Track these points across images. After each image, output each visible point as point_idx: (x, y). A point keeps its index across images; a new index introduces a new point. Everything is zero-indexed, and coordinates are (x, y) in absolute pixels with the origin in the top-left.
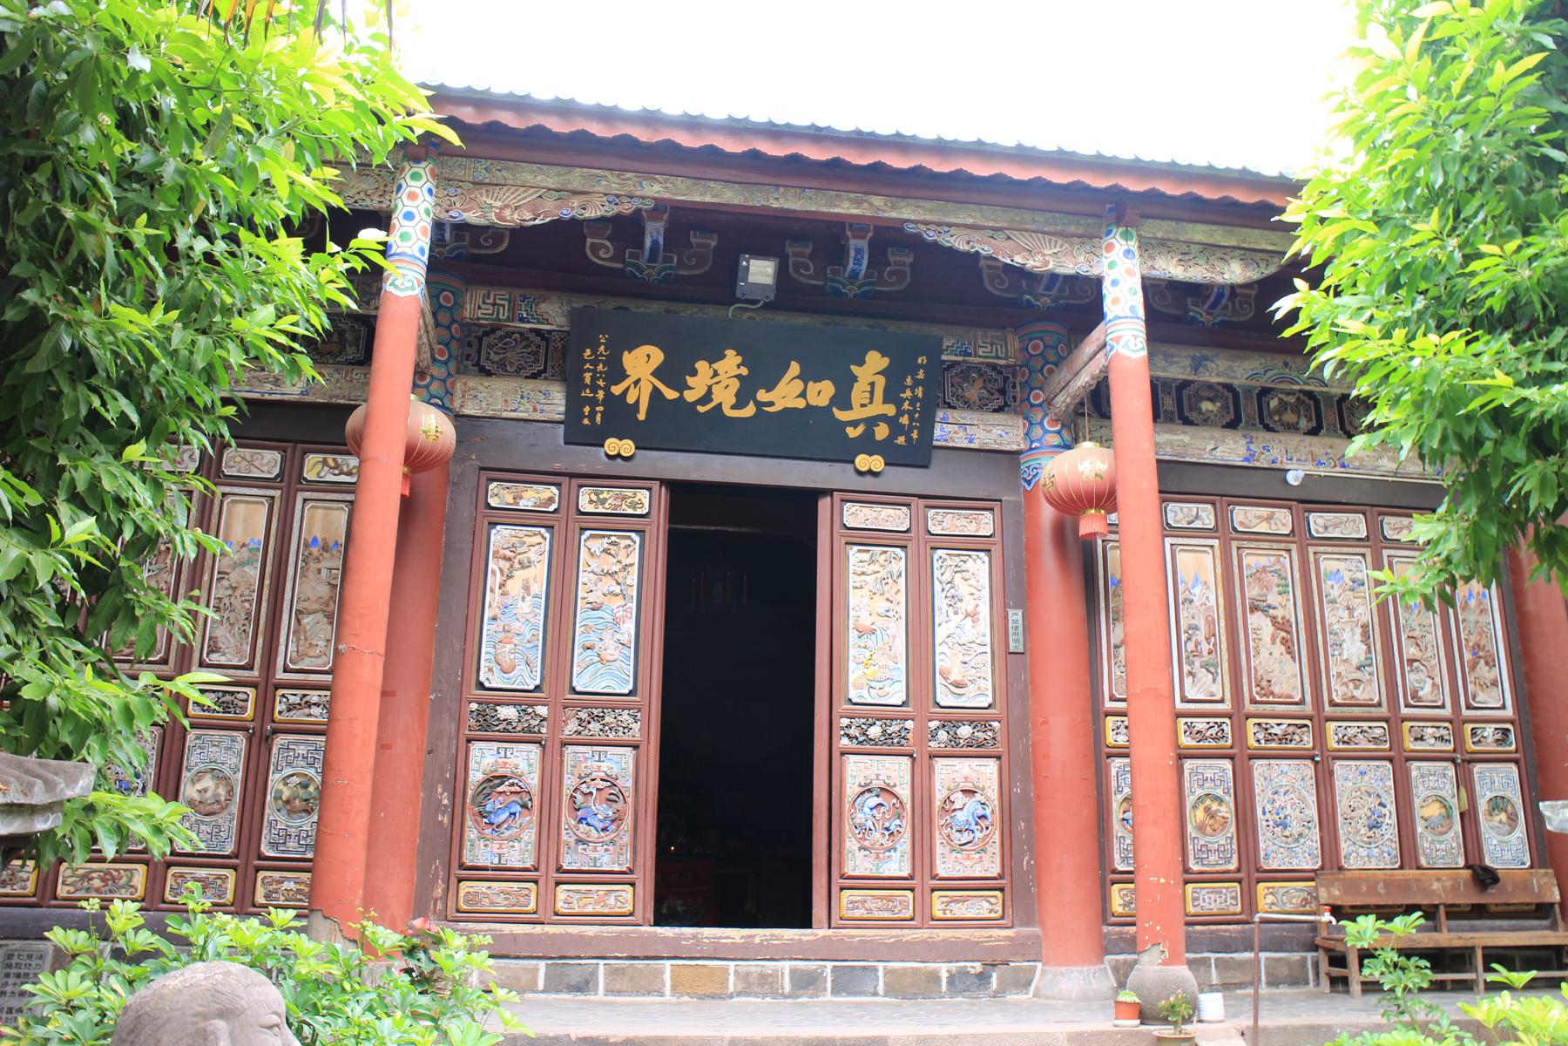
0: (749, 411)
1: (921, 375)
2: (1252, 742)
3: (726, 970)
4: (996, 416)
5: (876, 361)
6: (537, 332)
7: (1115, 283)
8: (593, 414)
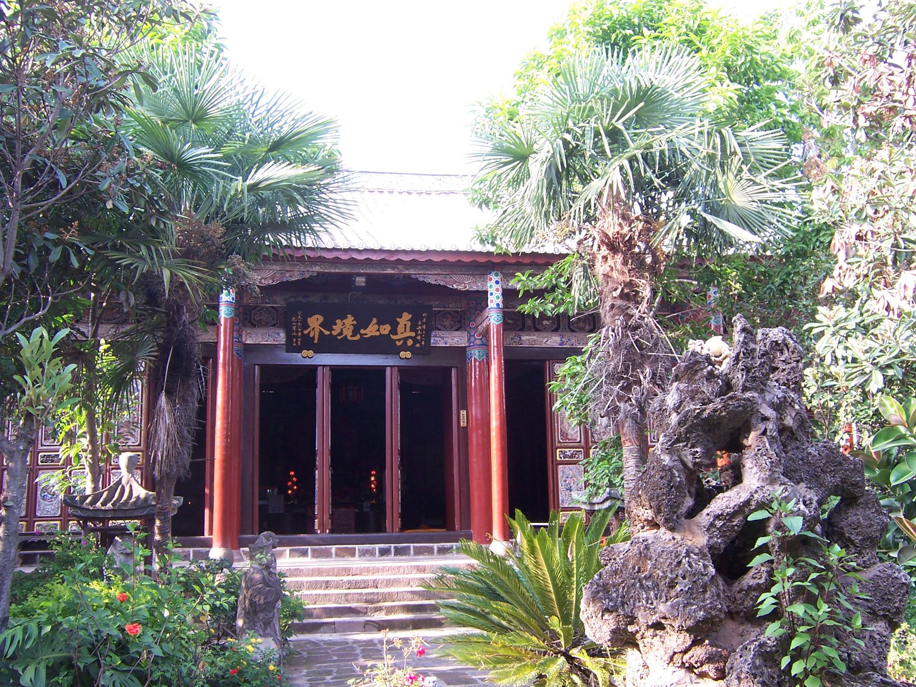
0: (358, 337)
1: (424, 320)
2: (558, 458)
3: (355, 549)
4: (456, 332)
5: (406, 316)
6: (273, 307)
7: (492, 294)
8: (297, 342)
